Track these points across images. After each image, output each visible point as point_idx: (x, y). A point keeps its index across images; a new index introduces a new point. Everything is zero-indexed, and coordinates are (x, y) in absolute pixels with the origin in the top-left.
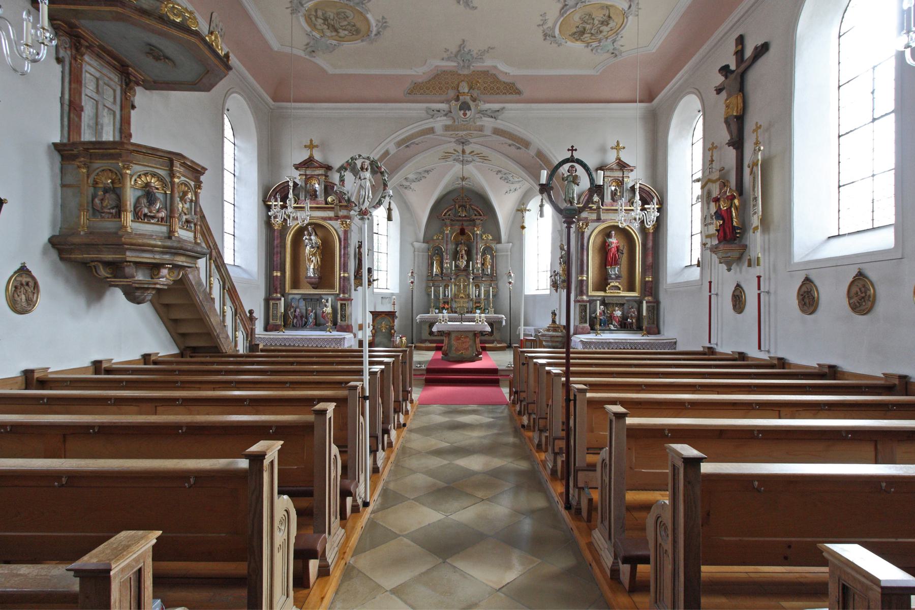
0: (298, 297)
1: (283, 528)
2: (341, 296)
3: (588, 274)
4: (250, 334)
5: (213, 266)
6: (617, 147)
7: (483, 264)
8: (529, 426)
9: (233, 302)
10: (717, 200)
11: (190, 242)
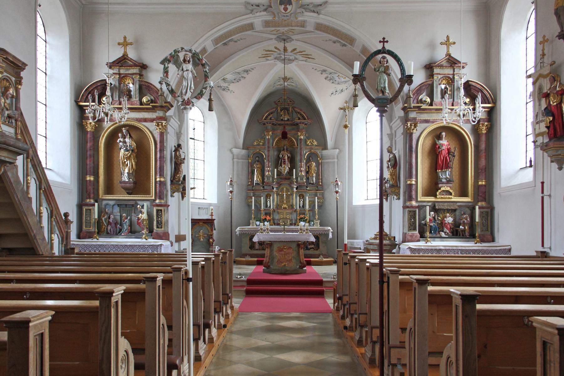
0: (112, 203)
1: (124, 366)
2: (157, 201)
3: (417, 178)
4: (65, 238)
5: (30, 165)
6: (447, 43)
7: (307, 172)
8: (351, 327)
9: (49, 203)
10: (547, 96)
11: (12, 137)
